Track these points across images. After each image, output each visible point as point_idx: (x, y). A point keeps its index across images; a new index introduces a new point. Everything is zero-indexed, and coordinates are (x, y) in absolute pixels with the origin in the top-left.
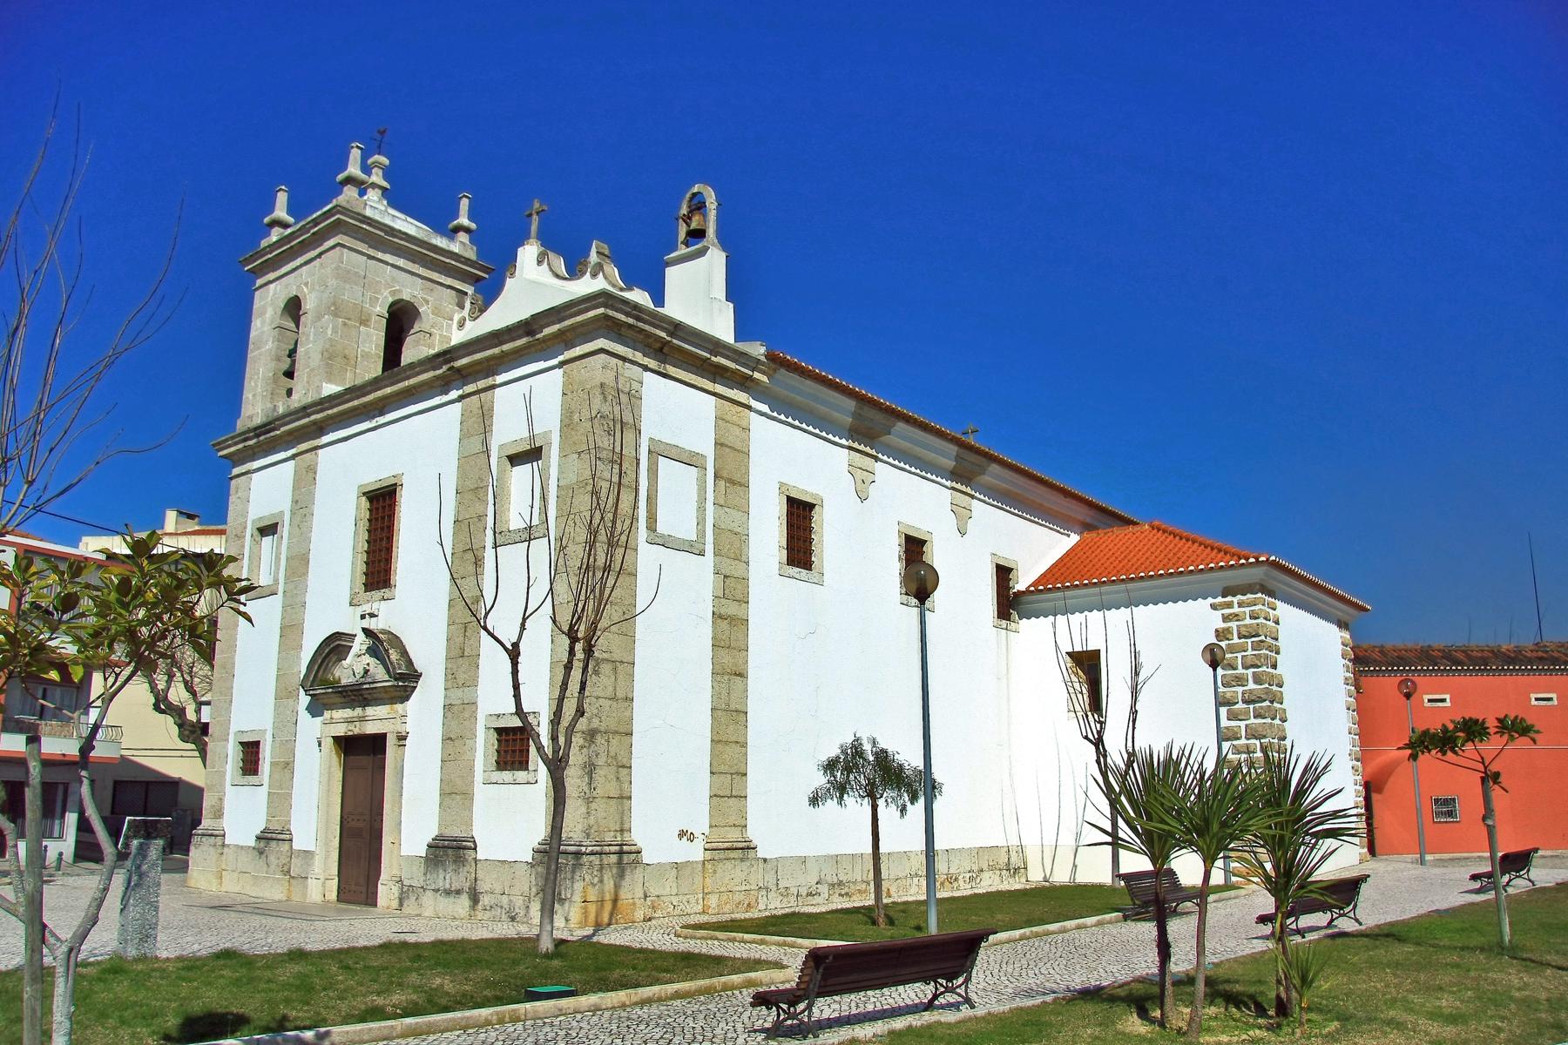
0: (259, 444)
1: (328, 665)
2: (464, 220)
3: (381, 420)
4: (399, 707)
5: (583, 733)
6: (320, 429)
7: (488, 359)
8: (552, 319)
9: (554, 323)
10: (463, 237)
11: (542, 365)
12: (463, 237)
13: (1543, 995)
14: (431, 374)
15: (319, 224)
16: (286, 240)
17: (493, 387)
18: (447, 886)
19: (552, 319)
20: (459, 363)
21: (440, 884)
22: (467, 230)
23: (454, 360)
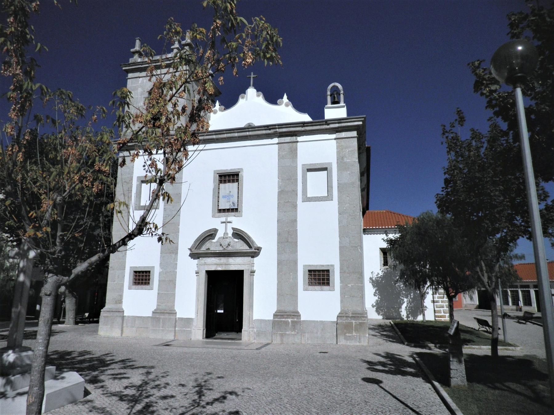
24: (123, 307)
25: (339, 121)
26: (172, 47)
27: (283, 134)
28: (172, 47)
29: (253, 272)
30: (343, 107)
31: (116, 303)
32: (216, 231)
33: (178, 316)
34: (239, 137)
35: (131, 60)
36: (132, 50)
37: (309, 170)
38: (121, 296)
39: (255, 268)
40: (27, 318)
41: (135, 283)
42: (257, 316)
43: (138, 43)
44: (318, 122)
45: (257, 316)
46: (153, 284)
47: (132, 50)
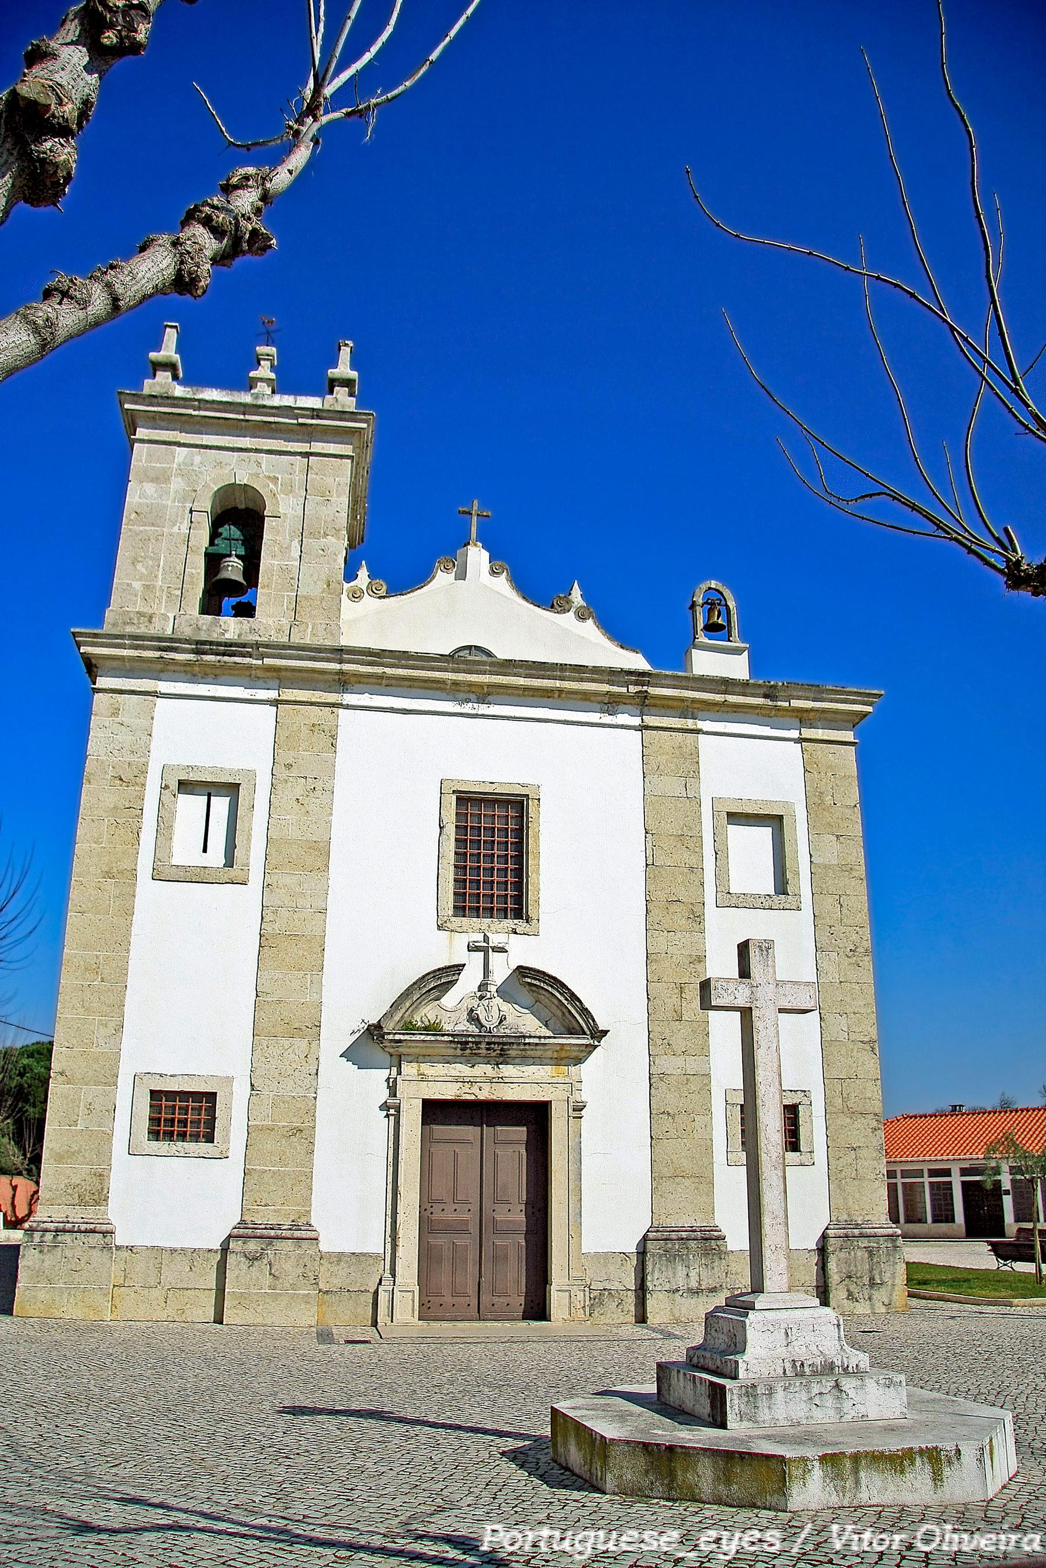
0: (188, 664)
1: (421, 1003)
2: (343, 369)
3: (483, 709)
4: (572, 1069)
5: (876, 1115)
6: (343, 682)
7: (694, 701)
8: (808, 695)
9: (807, 699)
10: (341, 392)
11: (767, 731)
12: (341, 392)
13: (304, 129)
14: (605, 688)
15: (319, 417)
16: (242, 409)
17: (698, 731)
18: (694, 1284)
19: (808, 695)
20: (652, 691)
21: (680, 1282)
22: (348, 383)
23: (648, 684)
24: (110, 1216)
25: (726, 685)
26: (252, 374)
27: (670, 703)
28: (252, 374)
29: (579, 1108)
30: (737, 651)
31: (82, 1202)
32: (459, 968)
33: (324, 1246)
34: (526, 688)
35: (150, 386)
36: (153, 355)
37: (735, 818)
38: (102, 1177)
39: (585, 1096)
40: (950, 1176)
41: (158, 1133)
42: (591, 1243)
43: (171, 337)
44: (290, 657)
45: (591, 1243)
46: (226, 1139)
47: (153, 355)
